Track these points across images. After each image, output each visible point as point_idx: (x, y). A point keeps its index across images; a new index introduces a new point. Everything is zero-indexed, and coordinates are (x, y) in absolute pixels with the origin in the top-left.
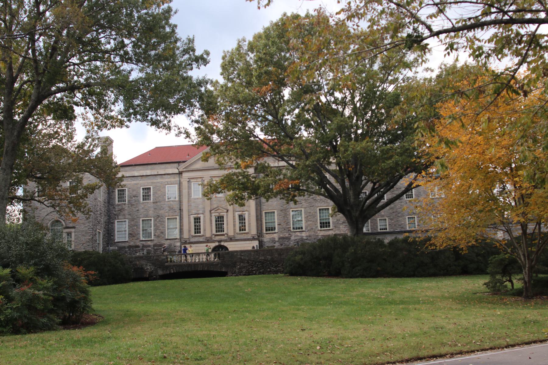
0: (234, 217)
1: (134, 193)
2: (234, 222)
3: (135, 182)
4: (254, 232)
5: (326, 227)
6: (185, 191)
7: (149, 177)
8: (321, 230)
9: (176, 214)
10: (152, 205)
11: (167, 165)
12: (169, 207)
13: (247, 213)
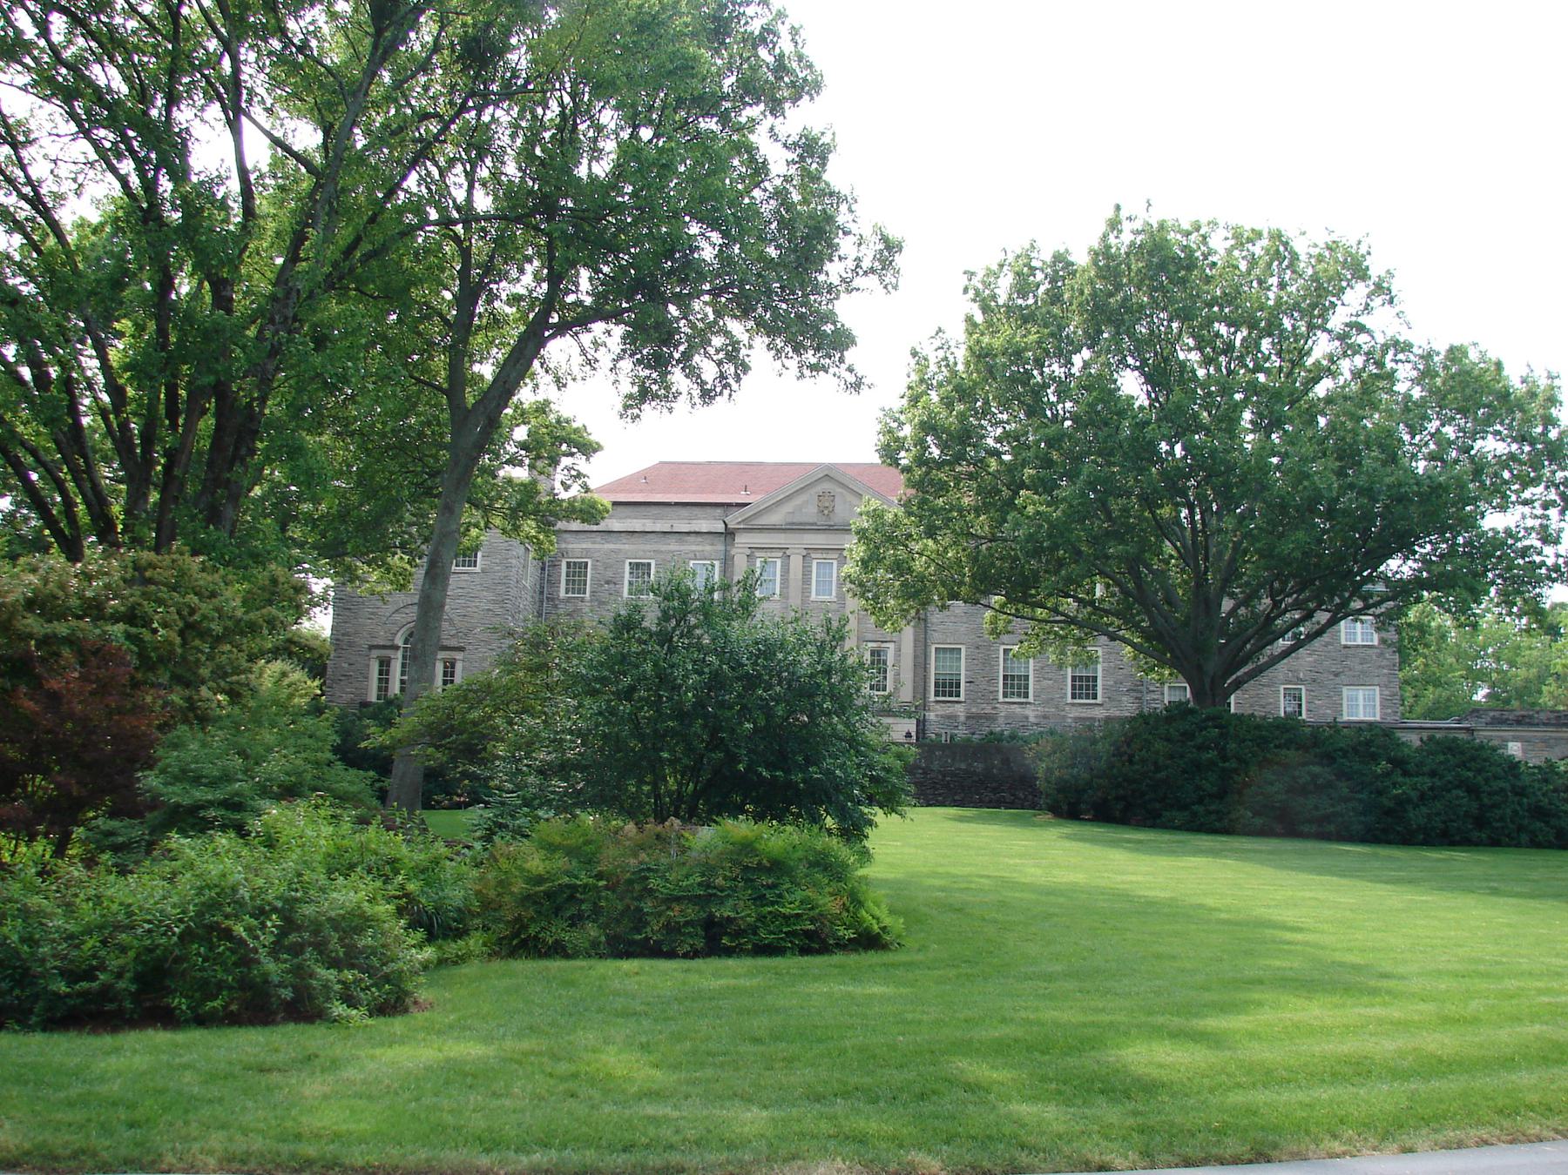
1: (609, 574)
3: (612, 546)
4: (906, 694)
5: (1088, 698)
7: (650, 536)
8: (1073, 705)
11: (696, 511)
13: (891, 646)
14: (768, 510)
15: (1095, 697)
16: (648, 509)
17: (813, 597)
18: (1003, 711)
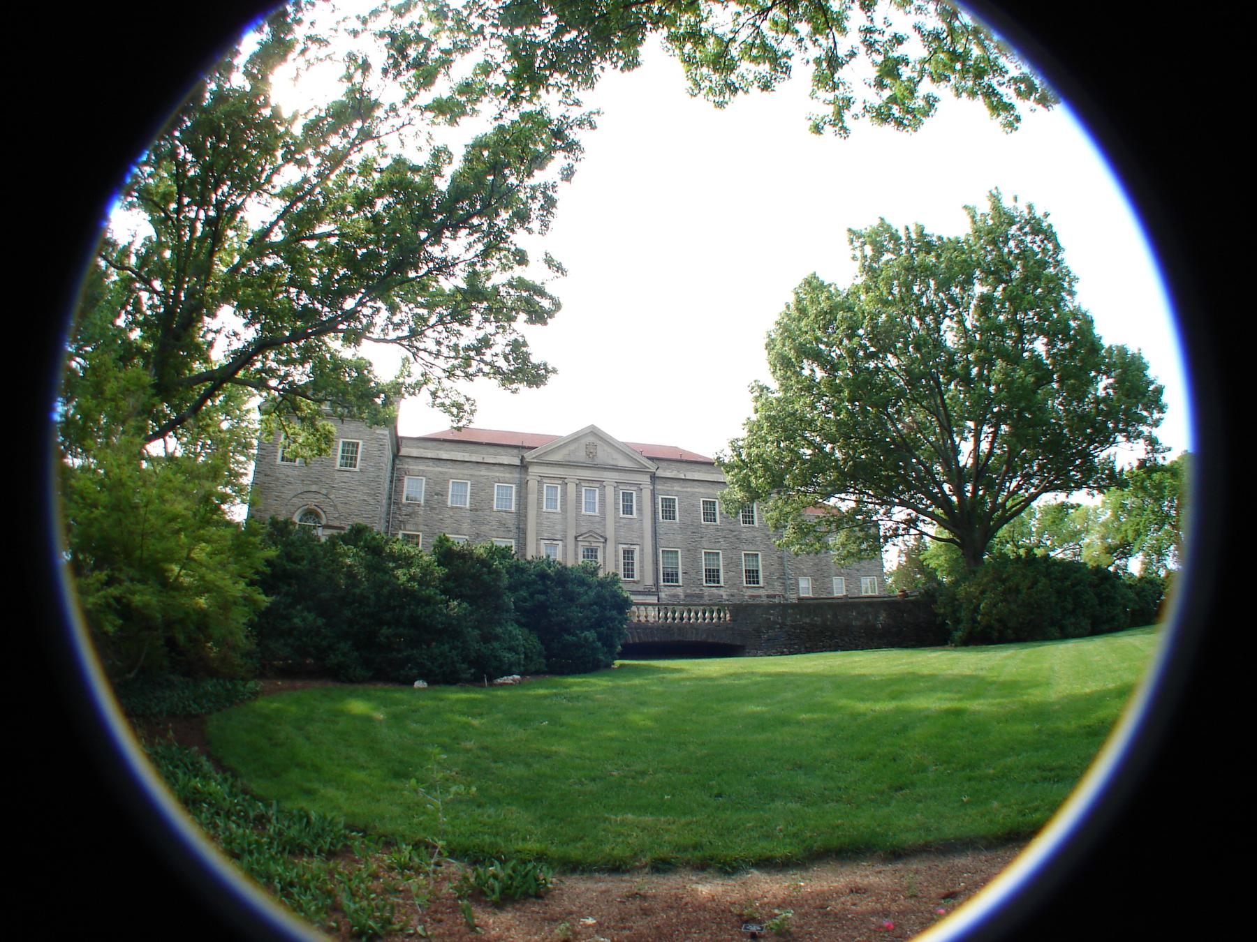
0: (616, 551)
1: (438, 488)
2: (617, 561)
3: (440, 469)
4: (649, 581)
6: (532, 498)
9: (511, 535)
10: (468, 514)
11: (500, 450)
12: (499, 522)
13: (637, 547)
14: (553, 451)
15: (758, 583)
16: (467, 446)
17: (583, 512)
18: (707, 592)
